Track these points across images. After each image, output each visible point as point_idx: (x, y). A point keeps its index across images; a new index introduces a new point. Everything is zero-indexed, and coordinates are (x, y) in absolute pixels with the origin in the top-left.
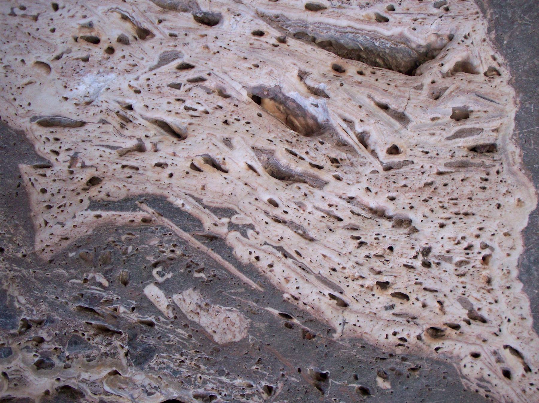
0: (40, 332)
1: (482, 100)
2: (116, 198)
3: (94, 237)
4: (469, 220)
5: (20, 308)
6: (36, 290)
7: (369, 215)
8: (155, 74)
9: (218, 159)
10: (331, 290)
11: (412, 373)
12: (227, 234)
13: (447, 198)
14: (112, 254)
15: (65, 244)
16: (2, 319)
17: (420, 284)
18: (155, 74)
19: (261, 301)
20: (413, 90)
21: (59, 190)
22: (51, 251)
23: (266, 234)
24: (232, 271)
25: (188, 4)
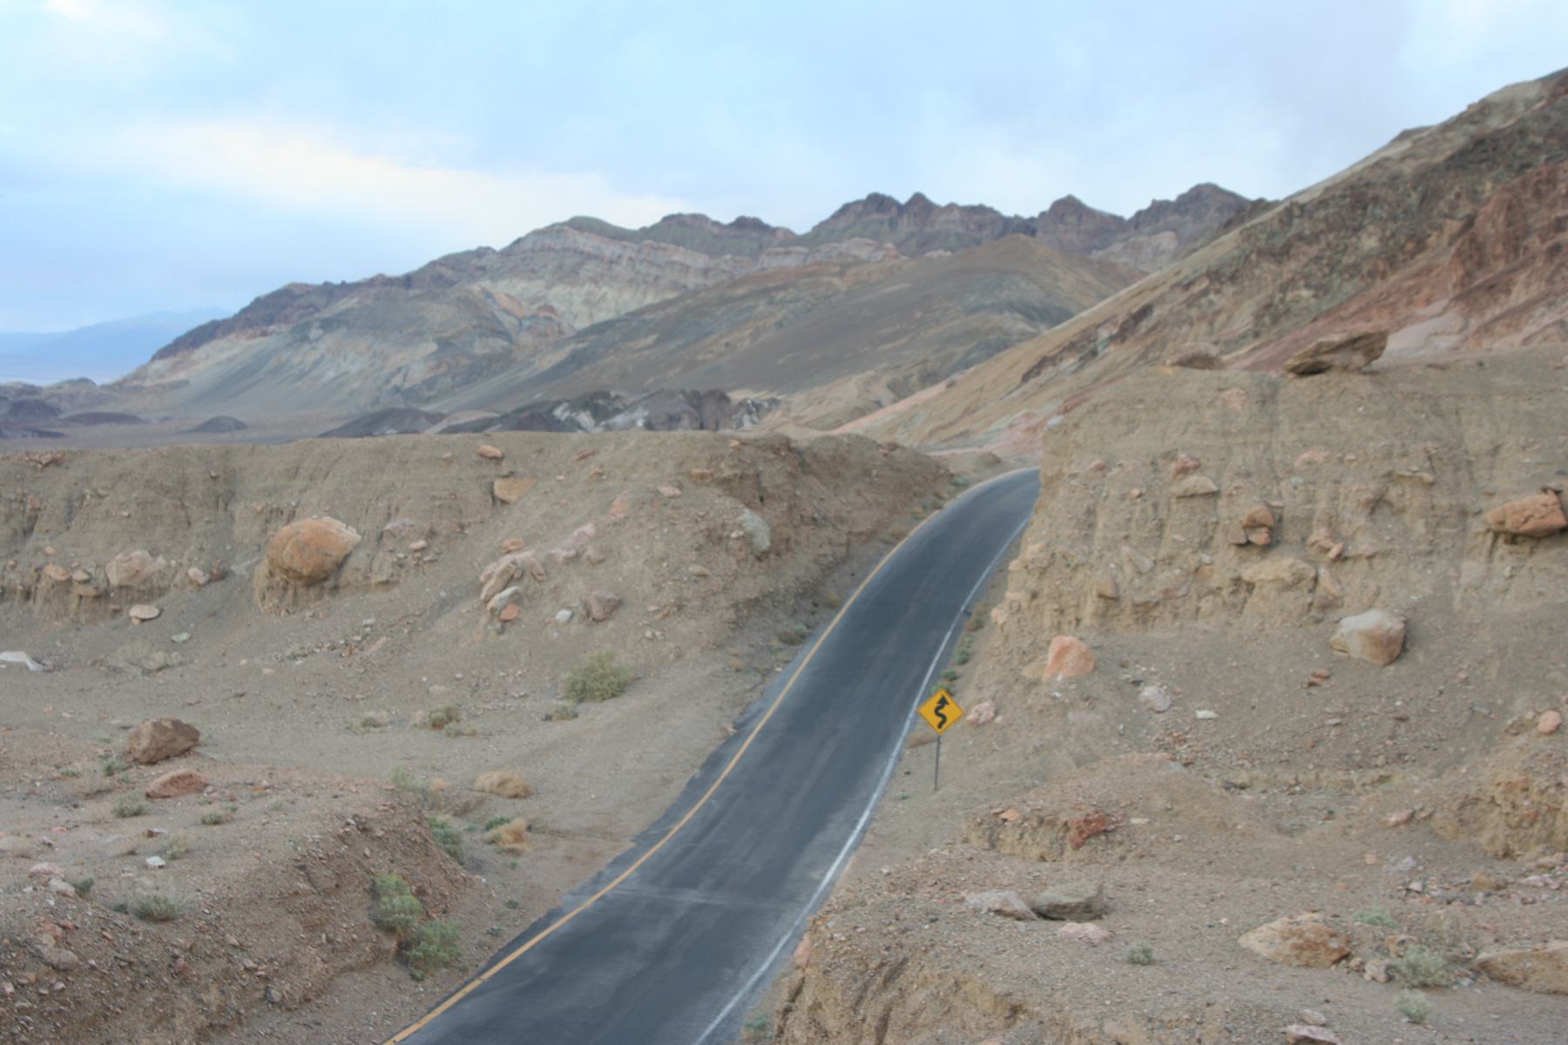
0: (1177, 571)
1: (934, 766)
2: (666, 781)
3: (1478, 673)
4: (512, 792)
5: (1415, 142)
6: (1291, 1023)
7: (1012, 1020)
8: (1416, 1020)
9: (1247, 568)
10: (860, 432)
11: (1214, 351)
12: (1247, 536)
13: (1043, 939)
14: (819, 923)
15: (1197, 341)
16: (10, 656)
17: (102, 662)
18: (1416, 1020)
19: (1385, 390)
20: (1333, 967)
21: (1134, 962)
22: (158, 889)
23: (447, 846)
24: (854, 842)
25: (1510, 826)
